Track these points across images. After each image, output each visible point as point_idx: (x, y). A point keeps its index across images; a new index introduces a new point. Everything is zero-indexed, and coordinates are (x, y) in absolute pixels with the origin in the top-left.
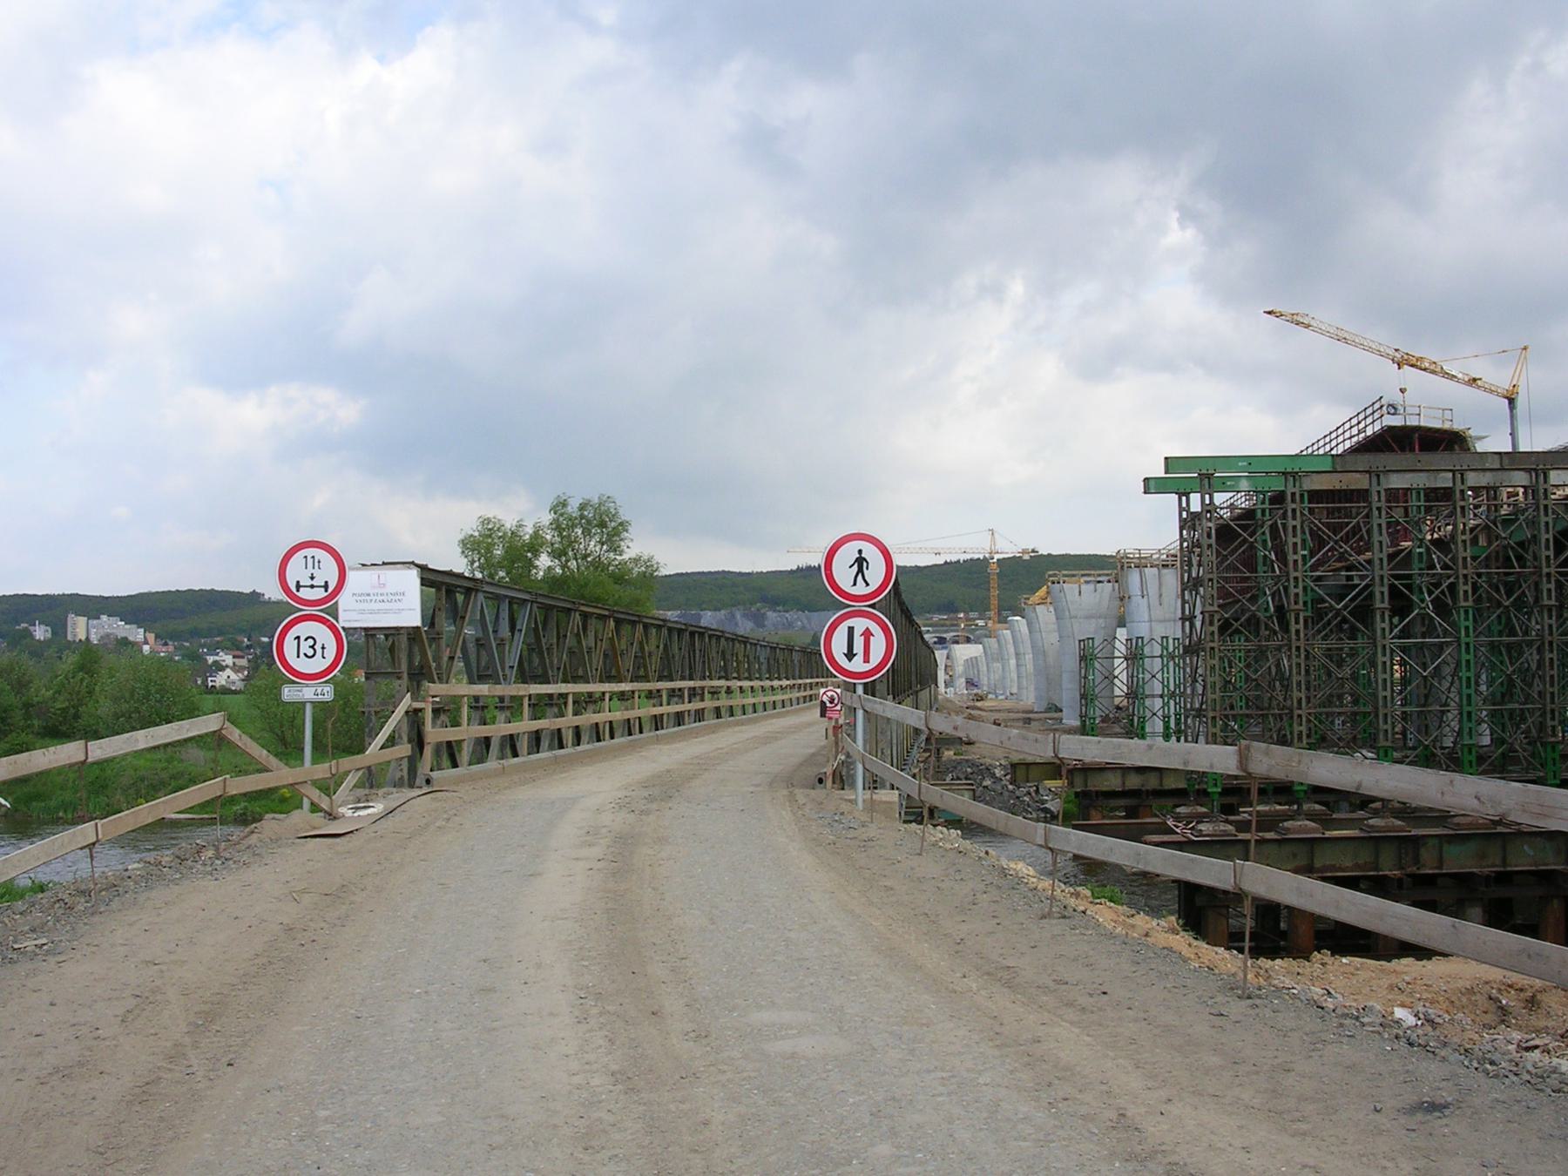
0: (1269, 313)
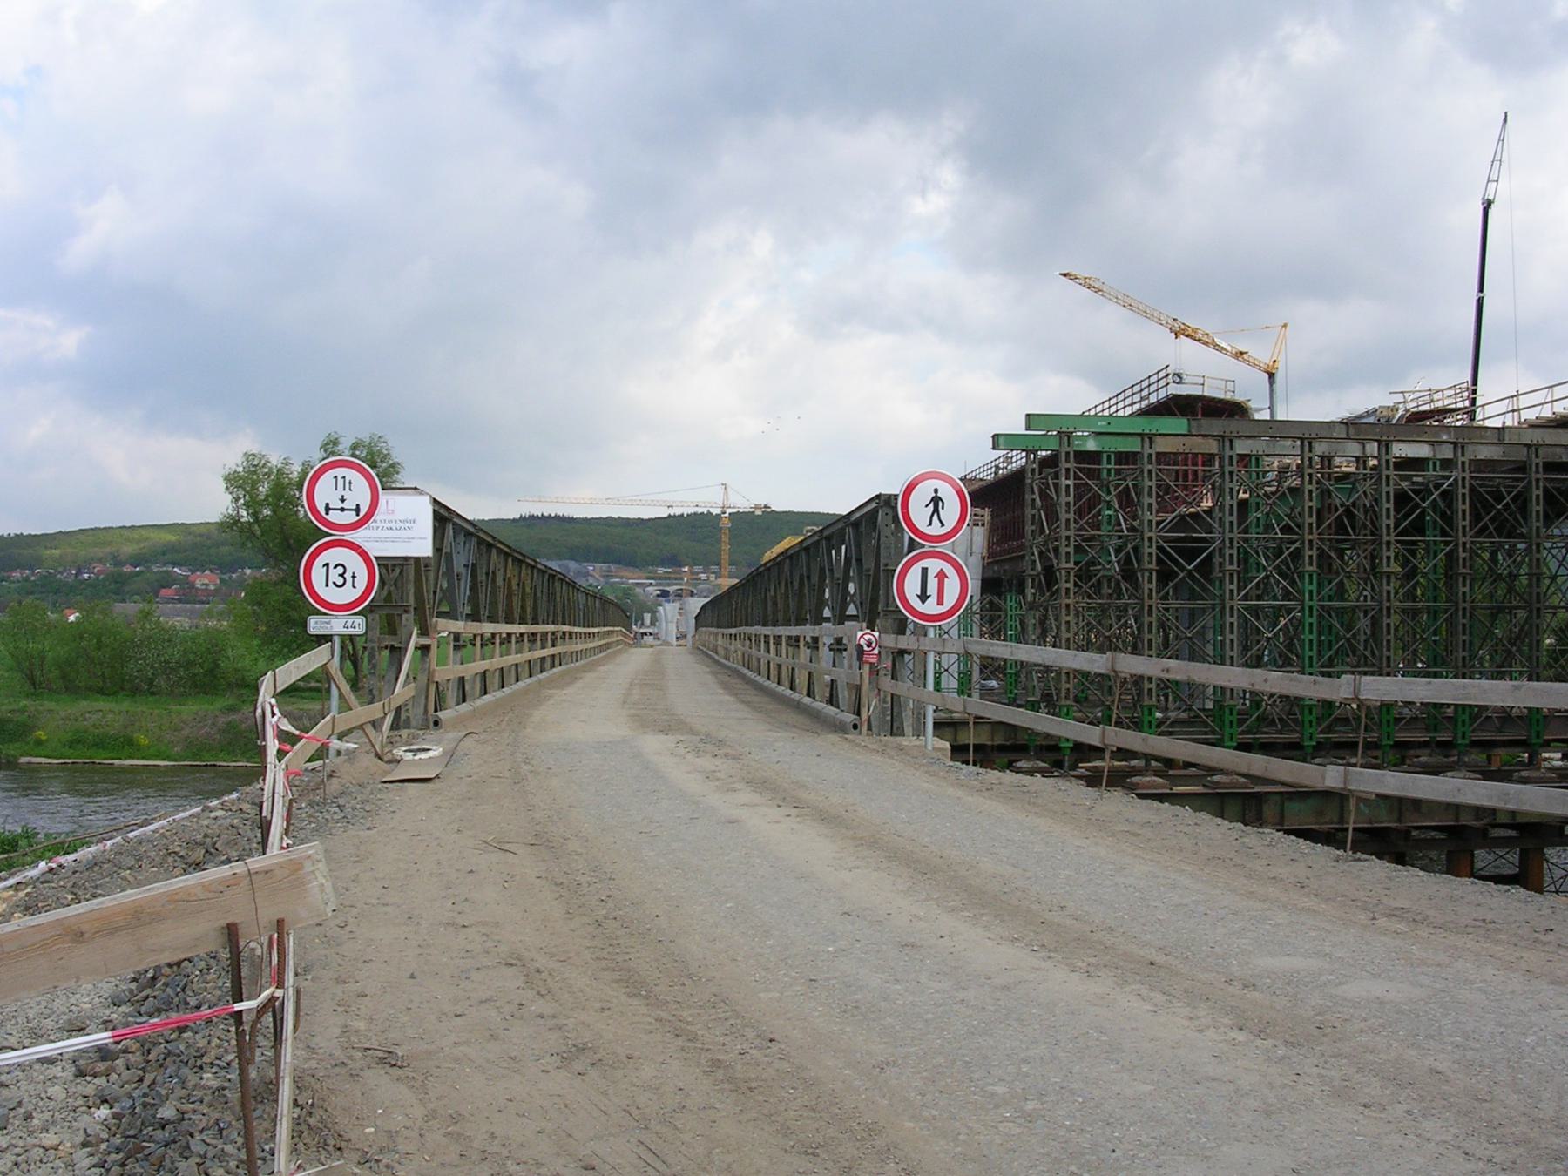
0: (1065, 275)
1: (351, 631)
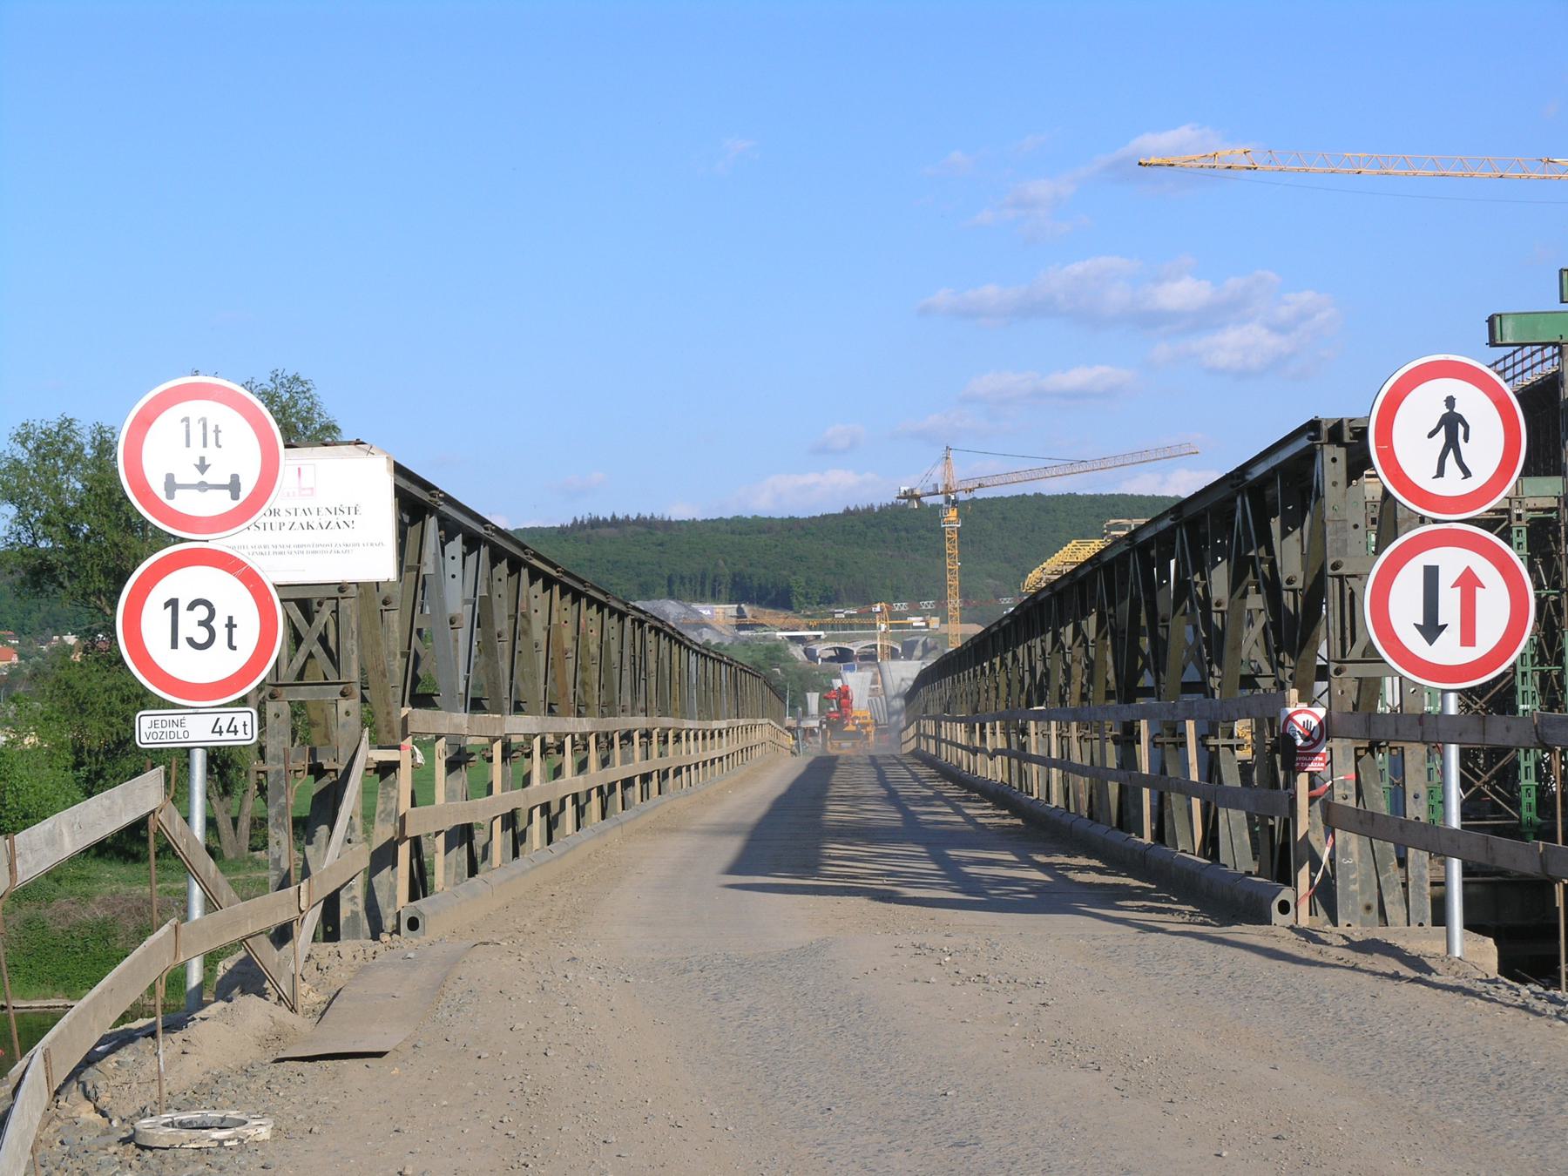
1: (227, 739)
